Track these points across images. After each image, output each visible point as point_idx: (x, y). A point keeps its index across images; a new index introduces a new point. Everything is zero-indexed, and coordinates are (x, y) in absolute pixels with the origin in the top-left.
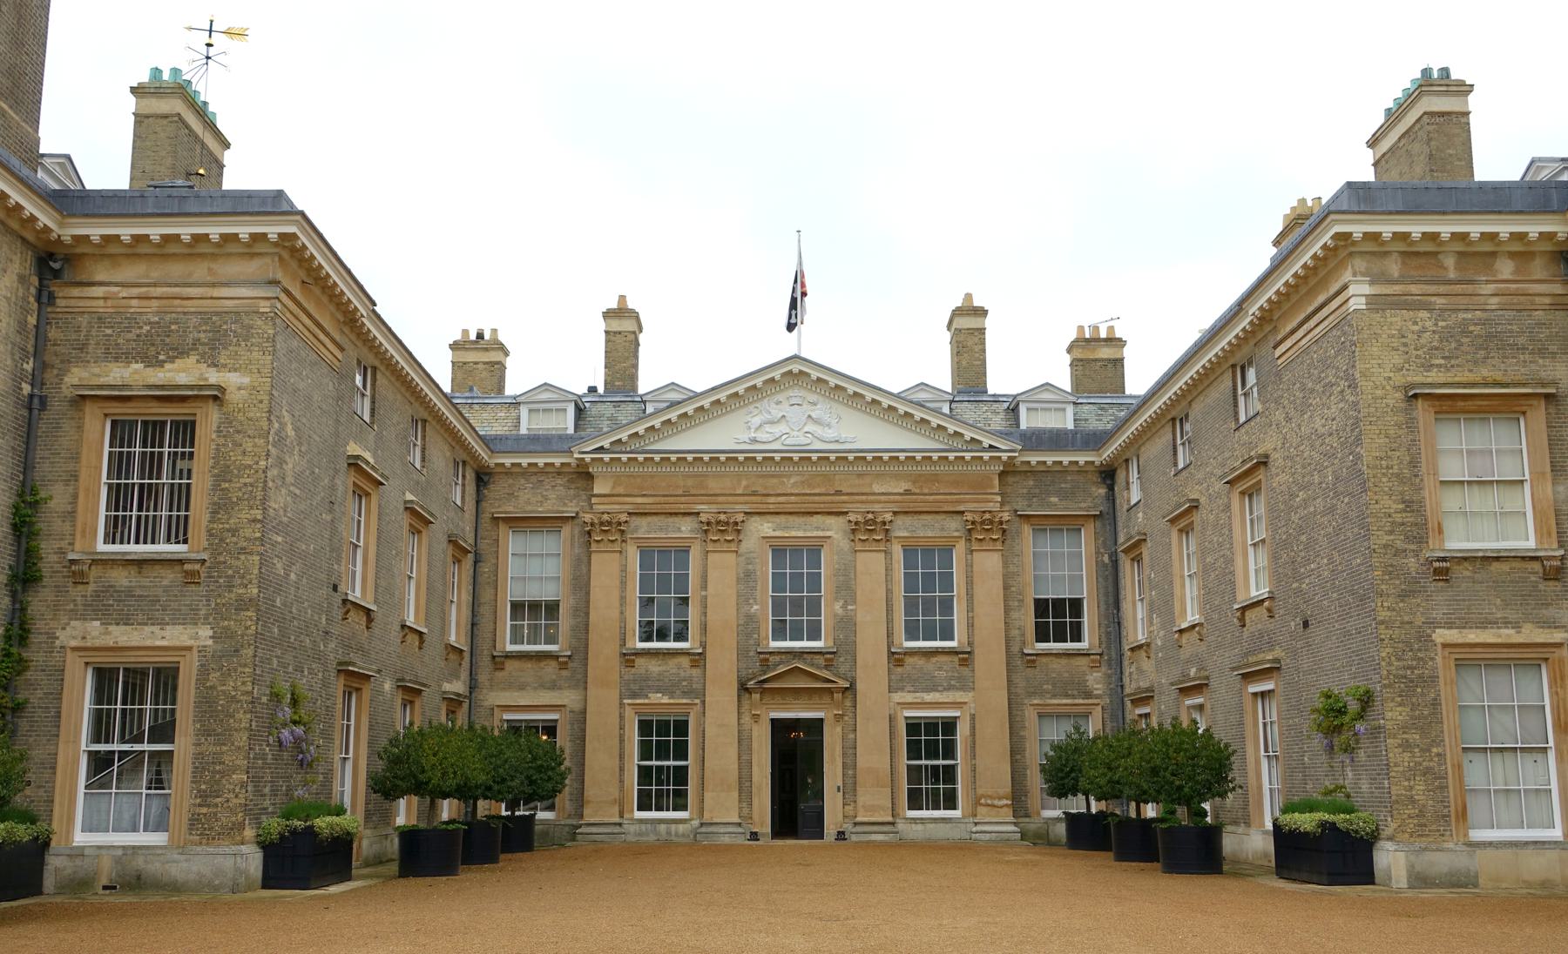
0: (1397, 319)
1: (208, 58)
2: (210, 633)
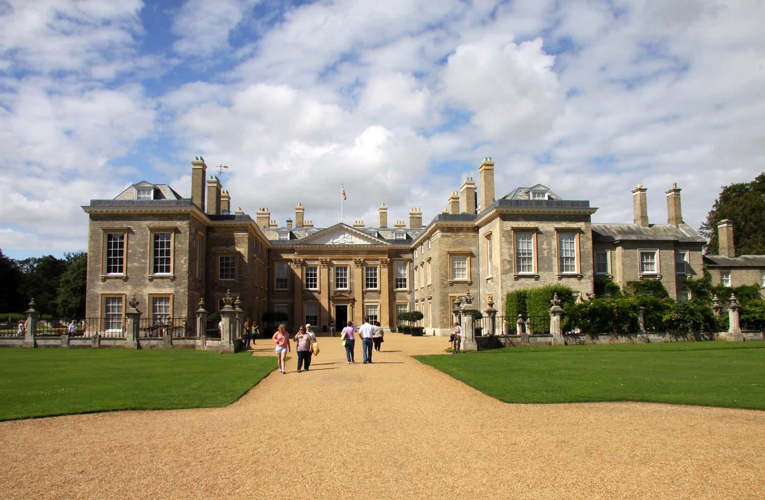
0: (446, 239)
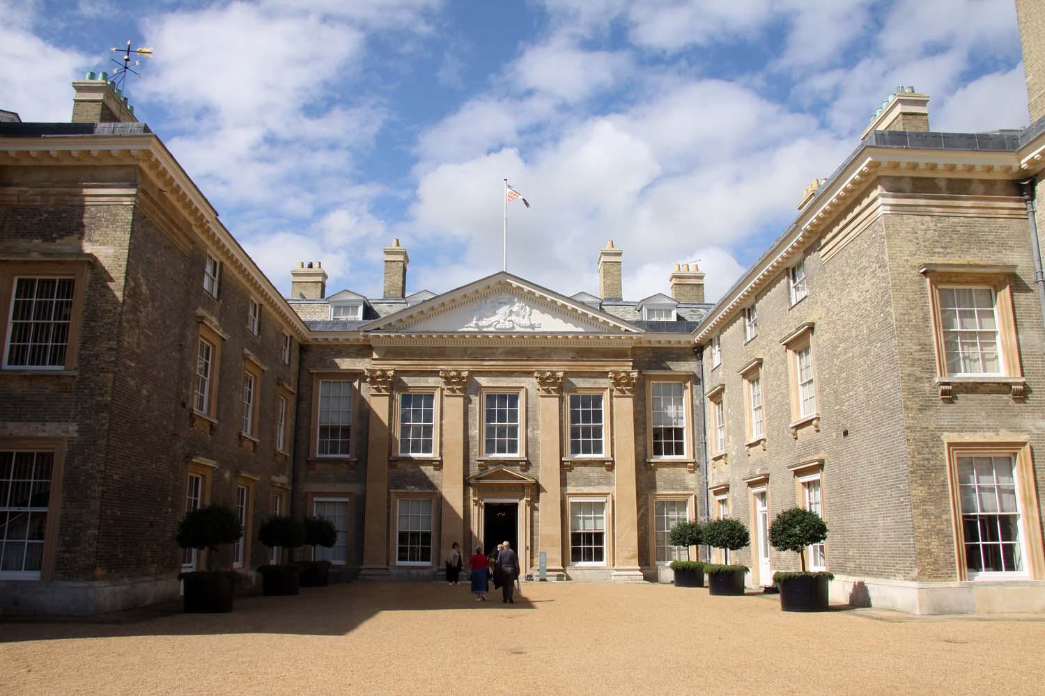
0: (912, 221)
1: (126, 68)
2: (77, 428)
